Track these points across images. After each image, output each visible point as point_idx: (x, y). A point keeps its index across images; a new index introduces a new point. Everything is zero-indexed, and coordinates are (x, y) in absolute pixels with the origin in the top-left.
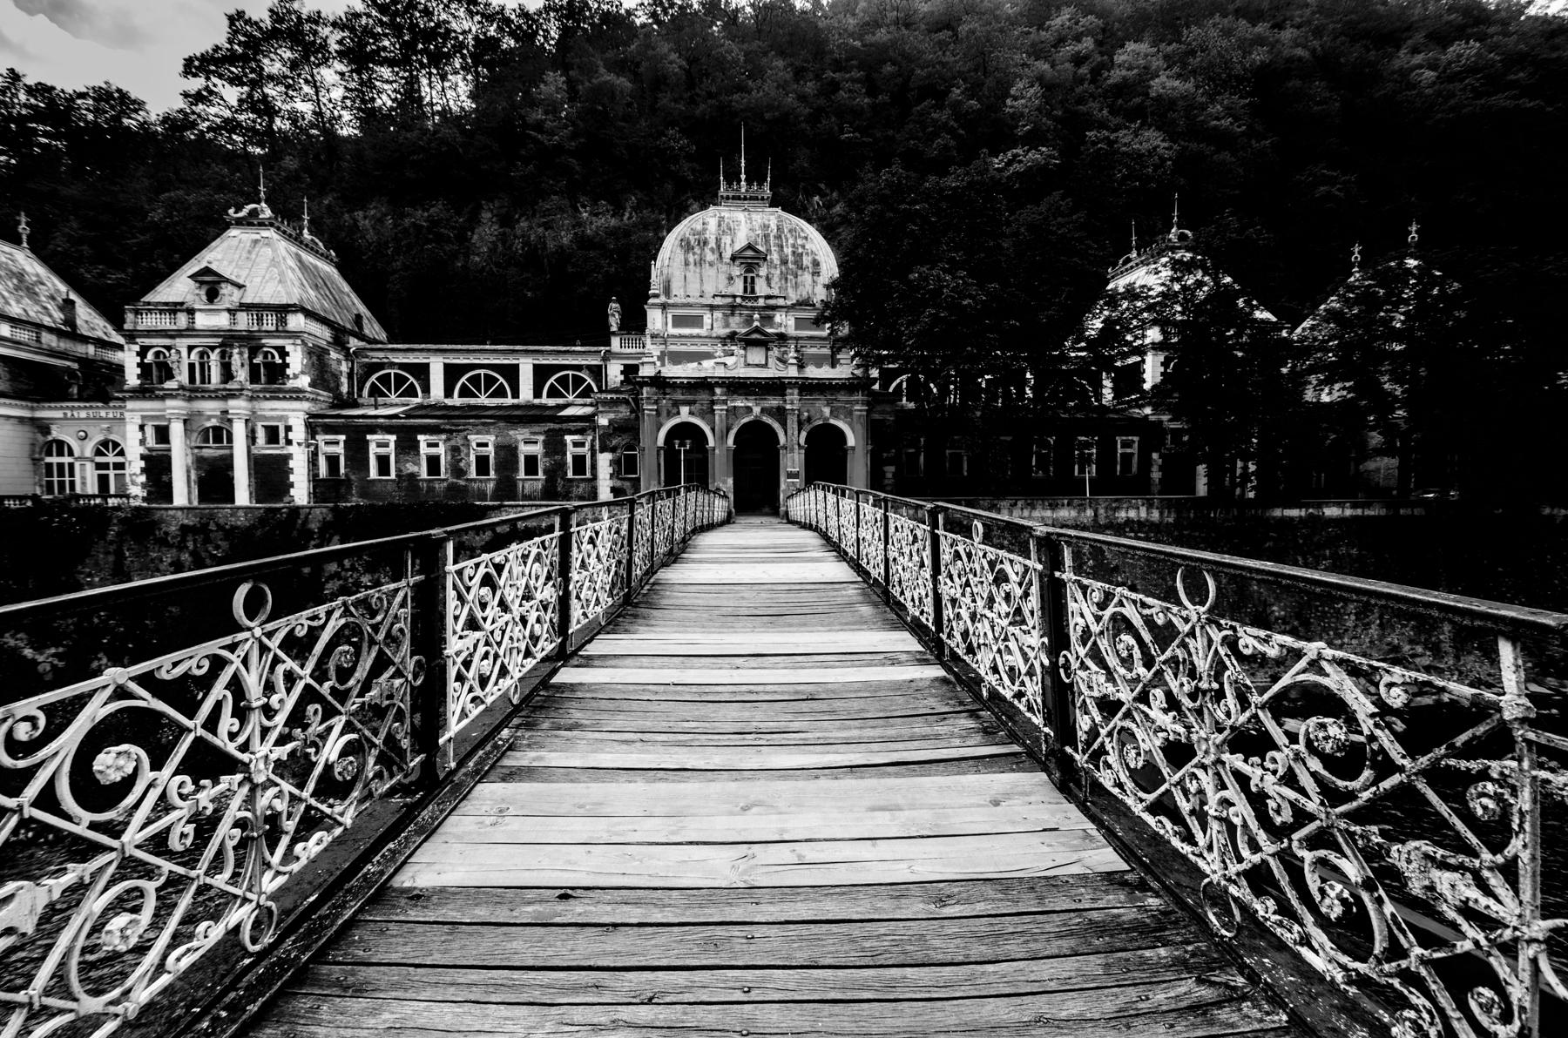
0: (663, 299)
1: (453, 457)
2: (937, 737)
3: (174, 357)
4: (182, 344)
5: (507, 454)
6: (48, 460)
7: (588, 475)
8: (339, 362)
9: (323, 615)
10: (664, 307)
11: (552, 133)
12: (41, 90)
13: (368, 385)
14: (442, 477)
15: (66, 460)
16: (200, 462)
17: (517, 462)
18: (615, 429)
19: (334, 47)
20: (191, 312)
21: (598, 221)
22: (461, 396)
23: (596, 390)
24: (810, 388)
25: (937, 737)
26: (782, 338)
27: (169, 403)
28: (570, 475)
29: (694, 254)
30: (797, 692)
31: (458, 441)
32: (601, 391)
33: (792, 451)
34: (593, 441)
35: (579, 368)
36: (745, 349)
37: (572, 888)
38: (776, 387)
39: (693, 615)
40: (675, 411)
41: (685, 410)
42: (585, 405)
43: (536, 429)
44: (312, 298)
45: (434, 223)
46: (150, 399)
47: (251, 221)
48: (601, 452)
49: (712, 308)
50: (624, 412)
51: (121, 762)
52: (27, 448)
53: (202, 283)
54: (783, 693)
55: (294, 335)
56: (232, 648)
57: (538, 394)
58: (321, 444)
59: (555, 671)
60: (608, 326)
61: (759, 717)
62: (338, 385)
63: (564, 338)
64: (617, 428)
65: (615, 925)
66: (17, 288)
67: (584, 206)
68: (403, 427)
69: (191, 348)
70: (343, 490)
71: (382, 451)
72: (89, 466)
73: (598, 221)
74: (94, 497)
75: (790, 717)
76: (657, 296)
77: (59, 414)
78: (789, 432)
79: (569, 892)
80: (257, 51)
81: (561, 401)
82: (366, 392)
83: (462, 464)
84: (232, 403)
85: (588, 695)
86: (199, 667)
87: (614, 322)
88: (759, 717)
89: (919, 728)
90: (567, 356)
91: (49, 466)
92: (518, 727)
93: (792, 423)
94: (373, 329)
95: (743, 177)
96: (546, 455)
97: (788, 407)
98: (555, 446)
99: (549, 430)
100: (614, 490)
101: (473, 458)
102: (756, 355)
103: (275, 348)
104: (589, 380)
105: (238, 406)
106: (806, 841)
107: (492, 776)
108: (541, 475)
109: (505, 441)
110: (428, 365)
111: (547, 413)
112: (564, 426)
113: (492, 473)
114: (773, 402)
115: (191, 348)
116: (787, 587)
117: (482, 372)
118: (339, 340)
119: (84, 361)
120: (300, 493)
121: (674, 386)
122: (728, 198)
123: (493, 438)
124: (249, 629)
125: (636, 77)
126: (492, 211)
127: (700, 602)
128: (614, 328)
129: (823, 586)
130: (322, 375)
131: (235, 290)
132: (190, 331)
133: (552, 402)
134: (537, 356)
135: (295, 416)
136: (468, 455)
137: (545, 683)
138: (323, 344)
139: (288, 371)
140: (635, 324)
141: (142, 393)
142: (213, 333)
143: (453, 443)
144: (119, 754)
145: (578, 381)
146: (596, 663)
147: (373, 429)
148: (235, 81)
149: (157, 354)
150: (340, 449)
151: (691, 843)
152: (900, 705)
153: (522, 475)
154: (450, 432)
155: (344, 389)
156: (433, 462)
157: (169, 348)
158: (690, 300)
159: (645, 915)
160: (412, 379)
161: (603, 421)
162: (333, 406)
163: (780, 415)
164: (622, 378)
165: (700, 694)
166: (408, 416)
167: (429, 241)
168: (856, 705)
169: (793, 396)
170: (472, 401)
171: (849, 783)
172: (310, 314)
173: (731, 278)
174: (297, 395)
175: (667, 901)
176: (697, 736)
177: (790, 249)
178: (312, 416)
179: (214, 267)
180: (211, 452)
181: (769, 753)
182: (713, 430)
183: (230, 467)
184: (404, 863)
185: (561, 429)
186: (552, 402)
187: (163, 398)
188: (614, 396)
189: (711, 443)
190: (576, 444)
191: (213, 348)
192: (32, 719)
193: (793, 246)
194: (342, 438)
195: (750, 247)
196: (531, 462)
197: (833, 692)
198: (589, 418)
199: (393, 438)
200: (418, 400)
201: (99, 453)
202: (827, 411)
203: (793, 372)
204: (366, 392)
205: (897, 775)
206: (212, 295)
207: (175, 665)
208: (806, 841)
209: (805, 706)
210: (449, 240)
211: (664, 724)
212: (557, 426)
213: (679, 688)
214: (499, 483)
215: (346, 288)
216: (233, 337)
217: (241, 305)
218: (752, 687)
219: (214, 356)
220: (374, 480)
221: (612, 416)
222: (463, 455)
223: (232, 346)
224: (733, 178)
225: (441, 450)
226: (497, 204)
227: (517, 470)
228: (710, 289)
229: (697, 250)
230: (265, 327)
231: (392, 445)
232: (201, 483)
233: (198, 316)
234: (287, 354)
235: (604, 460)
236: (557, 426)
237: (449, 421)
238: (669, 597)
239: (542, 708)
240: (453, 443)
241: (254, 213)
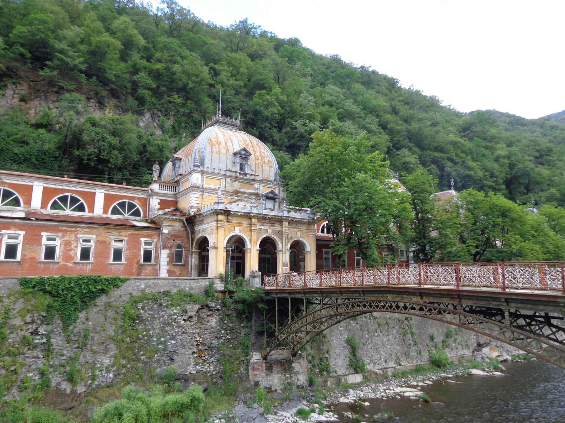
1: (65, 247)
7: (153, 262)
14: (56, 260)
24: (293, 222)
29: (216, 148)
34: (157, 242)
35: (133, 198)
38: (279, 220)
48: (163, 249)
57: (105, 212)
83: (71, 253)
91: (269, 254)
99: (131, 234)
100: (169, 271)
102: (270, 204)
104: (138, 206)
109: (102, 239)
110: (33, 186)
112: (141, 232)
123: (94, 237)
136: (76, 247)
143: (67, 238)
145: (131, 206)
153: (111, 261)
158: (215, 171)
160: (82, 201)
163: (280, 233)
169: (285, 224)
170: (61, 212)
190: (146, 243)
194: (126, 239)
202: (299, 234)
222: (73, 247)
225: (57, 243)
227: (108, 257)
228: (224, 168)
229: (217, 146)
231: (21, 238)
235: (164, 255)
240: (67, 238)
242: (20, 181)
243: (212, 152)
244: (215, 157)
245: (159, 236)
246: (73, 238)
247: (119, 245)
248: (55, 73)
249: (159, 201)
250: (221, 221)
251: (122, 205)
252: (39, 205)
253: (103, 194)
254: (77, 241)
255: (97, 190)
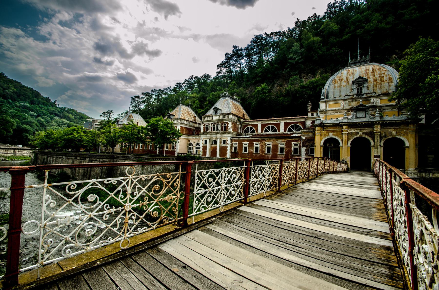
0: (325, 99)
1: (261, 148)
2: (362, 271)
3: (209, 126)
4: (210, 123)
5: (275, 146)
6: (189, 147)
7: (298, 154)
8: (239, 125)
9: (150, 176)
10: (326, 102)
11: (295, 59)
12: (196, 77)
13: (244, 130)
14: (259, 153)
15: (192, 147)
16: (211, 147)
17: (278, 149)
18: (307, 140)
19: (244, 54)
20: (212, 116)
21: (307, 81)
22: (288, 131)
23: (302, 128)
24: (385, 125)
25: (362, 271)
26: (374, 107)
27: (208, 135)
28: (293, 153)
30: (313, 233)
31: (263, 144)
32: (304, 129)
33: (377, 148)
34: (300, 144)
35: (298, 123)
36: (356, 112)
37: (188, 266)
38: (371, 125)
39: (298, 199)
40: (327, 134)
41: (331, 134)
42: (299, 133)
43: (284, 140)
44: (234, 111)
45: (263, 89)
46: (205, 134)
47: (225, 96)
48: (303, 147)
49: (344, 100)
50: (311, 134)
51: (92, 198)
52: (186, 144)
53: (215, 110)
54: (307, 232)
55: (230, 120)
56: (124, 180)
57: (285, 131)
58: (233, 144)
59: (240, 206)
60: (308, 110)
61: (290, 238)
62: (238, 131)
63: (293, 114)
64: (308, 140)
65: (187, 282)
66: (188, 115)
67: (303, 77)
68: (251, 140)
69: (212, 124)
70: (237, 155)
71: (245, 146)
72: (195, 148)
73: (307, 81)
74: (195, 154)
75: (302, 241)
76: (323, 99)
77: (191, 138)
78: (376, 141)
79: (186, 266)
80: (230, 60)
81: (292, 132)
82: (244, 132)
83: (264, 150)
84: (218, 135)
85: (243, 215)
86: (114, 182)
87: (309, 109)
88: (290, 238)
89: (356, 264)
90: (294, 120)
91: (189, 148)
92: (218, 218)
93: (377, 138)
94: (247, 117)
95: (359, 55)
96: (286, 147)
97: (375, 132)
98: (289, 145)
101: (266, 148)
102: (361, 114)
103: (226, 123)
104: (301, 126)
105: (219, 136)
106: (263, 286)
107: (200, 229)
108: (284, 153)
111: (287, 136)
112: (292, 139)
113: (271, 152)
114: (368, 130)
115: (212, 124)
116: (344, 196)
117: (270, 125)
118: (239, 121)
119: (196, 128)
120: (228, 155)
121: (327, 126)
122: (352, 64)
123: (272, 143)
124: (129, 176)
125: (322, 36)
126: (277, 83)
127: (305, 195)
128: (309, 110)
129: (361, 198)
130: (235, 128)
131: (220, 111)
132: (212, 121)
133: (289, 133)
134: (285, 120)
135: (228, 137)
136: (265, 147)
137: (235, 209)
138: (235, 121)
139: (228, 128)
140: (316, 108)
141: (204, 133)
142: (216, 120)
143: (262, 144)
144: (92, 196)
145: (297, 126)
146: (254, 207)
147: (244, 141)
148: (226, 67)
149: (206, 125)
150: (237, 145)
151: (228, 268)
152: (356, 253)
153: (279, 153)
154: (261, 141)
155: (239, 131)
156: (257, 149)
157: (208, 124)
159: (196, 283)
161: (304, 138)
162: (237, 135)
163: (372, 135)
164: (311, 125)
165: (277, 224)
166: (252, 137)
167: (261, 94)
168: (334, 245)
170: (268, 133)
171: (293, 271)
172: (233, 115)
173: (352, 89)
174: (229, 133)
175: (205, 282)
176: (264, 237)
177: (378, 76)
178: (232, 138)
179: (217, 107)
180: (213, 146)
181: (282, 251)
182: (342, 140)
183: (216, 149)
184: (164, 242)
185: (291, 140)
186: (289, 133)
187: (206, 134)
188: (308, 130)
189: (341, 145)
190: (295, 145)
191: (215, 124)
192: (74, 185)
193: (380, 74)
195: (360, 78)
196: (282, 149)
197: (328, 237)
198: (299, 137)
199: (248, 143)
200: (254, 133)
201: (196, 146)
202: (394, 133)
203: (378, 119)
204: (244, 132)
205: (326, 279)
206: (216, 113)
207: (108, 181)
208: (263, 286)
209: (312, 239)
210: (266, 93)
211: (257, 230)
212: (289, 139)
213: (272, 220)
214: (272, 155)
215: (242, 108)
216: (219, 121)
217: (221, 114)
218: (297, 227)
219: (216, 125)
220: (243, 153)
221: (307, 136)
223: (218, 123)
224: (354, 56)
225: (259, 146)
226: (279, 81)
227: (278, 152)
228: (343, 94)
229: (339, 82)
230: (225, 118)
231: (248, 144)
232: (211, 152)
233: (214, 117)
234: (228, 124)
235: (304, 150)
236: (289, 139)
237: (261, 138)
238: (296, 192)
239: (229, 215)
240: (262, 144)
241: (225, 94)
242: (254, 123)
243: (334, 87)
244: (337, 90)
245: (301, 141)
246: (264, 144)
247: (282, 146)
248: (288, 70)
249: (311, 122)
250: (318, 130)
251: (293, 127)
252: (260, 131)
253: (284, 123)
254: (265, 145)
255: (281, 122)
